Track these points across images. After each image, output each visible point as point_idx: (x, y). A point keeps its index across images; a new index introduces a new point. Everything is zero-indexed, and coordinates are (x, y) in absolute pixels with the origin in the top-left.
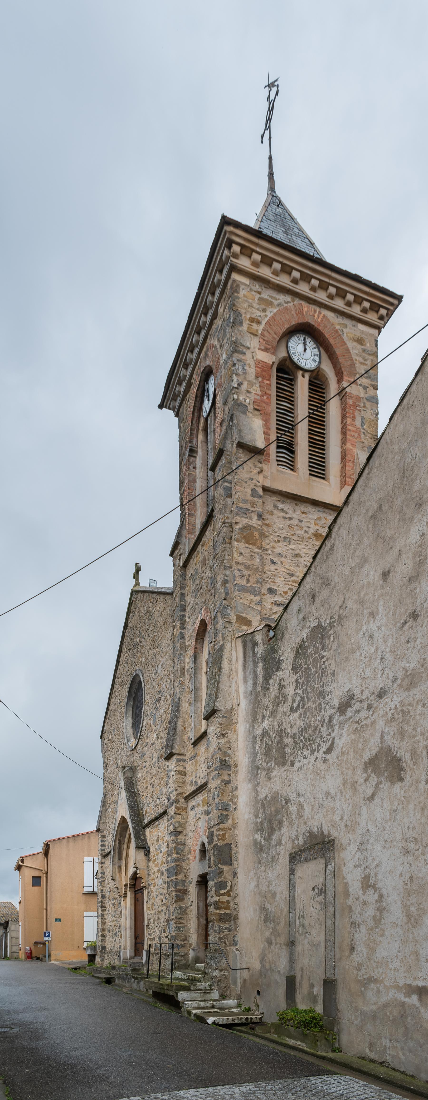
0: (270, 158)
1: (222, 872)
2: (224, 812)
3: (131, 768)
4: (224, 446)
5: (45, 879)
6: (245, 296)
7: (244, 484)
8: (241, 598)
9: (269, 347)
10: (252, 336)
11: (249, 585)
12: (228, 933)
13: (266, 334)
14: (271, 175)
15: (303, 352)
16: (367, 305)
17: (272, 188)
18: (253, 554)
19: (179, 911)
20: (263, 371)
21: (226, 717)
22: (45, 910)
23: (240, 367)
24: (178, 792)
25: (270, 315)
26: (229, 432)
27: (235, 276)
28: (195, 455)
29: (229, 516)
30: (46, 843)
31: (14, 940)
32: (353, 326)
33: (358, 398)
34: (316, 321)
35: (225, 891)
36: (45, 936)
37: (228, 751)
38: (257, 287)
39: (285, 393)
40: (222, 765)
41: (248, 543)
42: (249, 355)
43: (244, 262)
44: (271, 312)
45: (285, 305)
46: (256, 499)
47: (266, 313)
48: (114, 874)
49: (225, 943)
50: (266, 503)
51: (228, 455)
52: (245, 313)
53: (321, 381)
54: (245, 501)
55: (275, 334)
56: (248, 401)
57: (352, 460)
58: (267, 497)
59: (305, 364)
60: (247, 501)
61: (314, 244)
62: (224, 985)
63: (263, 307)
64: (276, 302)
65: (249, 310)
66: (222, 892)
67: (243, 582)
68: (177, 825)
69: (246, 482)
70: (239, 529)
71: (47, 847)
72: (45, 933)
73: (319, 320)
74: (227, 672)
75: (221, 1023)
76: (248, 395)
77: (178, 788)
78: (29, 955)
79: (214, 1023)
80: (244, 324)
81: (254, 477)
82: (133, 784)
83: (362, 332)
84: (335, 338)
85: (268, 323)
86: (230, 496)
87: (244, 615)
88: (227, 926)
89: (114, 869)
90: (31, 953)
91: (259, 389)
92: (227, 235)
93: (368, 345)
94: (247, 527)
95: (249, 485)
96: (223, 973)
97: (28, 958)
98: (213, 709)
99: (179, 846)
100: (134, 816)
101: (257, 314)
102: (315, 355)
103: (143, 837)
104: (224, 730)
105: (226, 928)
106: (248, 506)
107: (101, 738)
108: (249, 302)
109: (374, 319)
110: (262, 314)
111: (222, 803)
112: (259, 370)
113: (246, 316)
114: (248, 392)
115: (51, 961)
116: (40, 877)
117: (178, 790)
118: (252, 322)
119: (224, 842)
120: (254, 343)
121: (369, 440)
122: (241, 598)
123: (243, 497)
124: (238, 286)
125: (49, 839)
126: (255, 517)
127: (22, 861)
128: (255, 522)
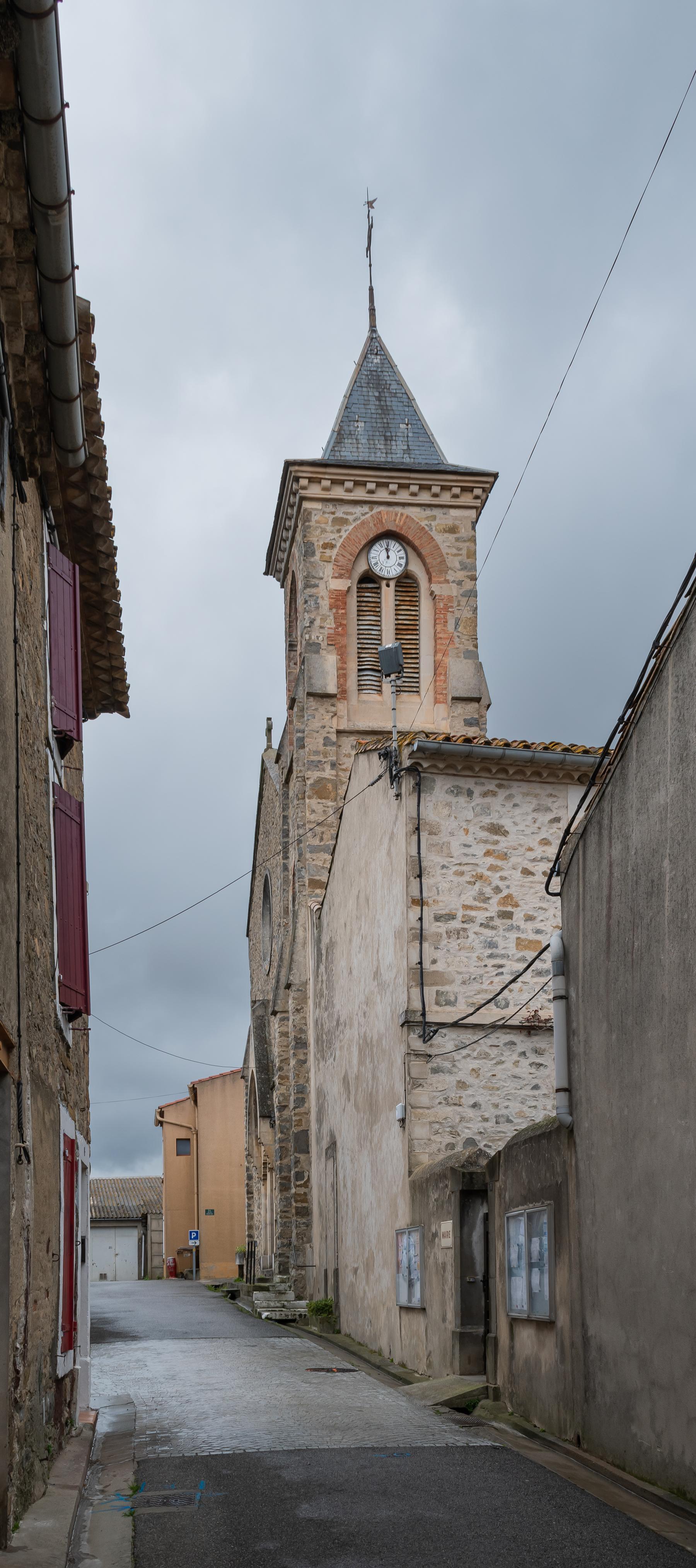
0: (371, 290)
1: (299, 1161)
2: (300, 1096)
3: (263, 1003)
4: (296, 695)
5: (195, 1142)
6: (317, 522)
7: (315, 735)
8: (313, 860)
9: (343, 572)
10: (325, 563)
11: (322, 843)
12: (305, 1228)
13: (340, 558)
14: (372, 310)
15: (386, 560)
16: (457, 491)
17: (373, 328)
18: (326, 809)
19: (285, 1203)
20: (337, 600)
21: (302, 991)
22: (196, 1195)
23: (313, 603)
24: (281, 1058)
25: (344, 535)
26: (301, 677)
27: (306, 505)
28: (295, 649)
29: (302, 768)
30: (191, 1086)
31: (155, 1247)
32: (444, 514)
33: (450, 598)
34: (397, 526)
35: (302, 1182)
36: (191, 1239)
37: (304, 1027)
38: (330, 508)
39: (369, 605)
40: (297, 1043)
41: (321, 798)
42: (322, 585)
43: (315, 491)
44: (346, 531)
45: (363, 518)
46: (329, 748)
47: (341, 534)
48: (250, 1148)
49: (302, 1239)
50: (343, 746)
51: (300, 702)
52: (318, 540)
53: (413, 580)
54: (317, 753)
55: (351, 555)
56: (321, 638)
57: (443, 672)
58: (345, 738)
59: (388, 572)
60: (319, 752)
61: (414, 399)
62: (301, 1285)
63: (338, 527)
64: (351, 518)
65: (323, 536)
66: (298, 1183)
67: (316, 842)
68: (281, 1099)
69: (318, 732)
70: (311, 785)
71: (194, 1090)
72: (191, 1232)
73: (402, 523)
74: (301, 941)
75: (274, 1318)
76: (322, 631)
77: (282, 1053)
78: (172, 1270)
79: (267, 1318)
80: (317, 553)
81: (326, 724)
82: (265, 1026)
83: (456, 518)
84: (421, 537)
85: (343, 546)
86: (303, 747)
87: (317, 878)
88: (304, 1220)
89: (250, 1141)
90: (175, 1267)
91: (333, 621)
92: (293, 474)
93: (463, 530)
94: (320, 780)
95: (321, 734)
96: (299, 1272)
97: (172, 1276)
98: (287, 984)
99: (283, 1124)
100: (262, 1072)
101: (330, 537)
102: (400, 558)
103: (269, 1103)
104: (299, 1005)
105: (304, 1223)
106: (321, 758)
107: (248, 936)
108: (321, 528)
109: (470, 501)
110: (336, 536)
111: (297, 1086)
112: (333, 601)
113: (318, 543)
114: (321, 627)
115: (200, 1279)
116: (189, 1140)
117: (282, 1056)
118: (325, 548)
119: (301, 1128)
120: (328, 570)
121: (466, 642)
122: (313, 860)
123: (315, 749)
124: (310, 514)
125: (196, 1079)
126: (328, 767)
127: (162, 1114)
128: (328, 773)
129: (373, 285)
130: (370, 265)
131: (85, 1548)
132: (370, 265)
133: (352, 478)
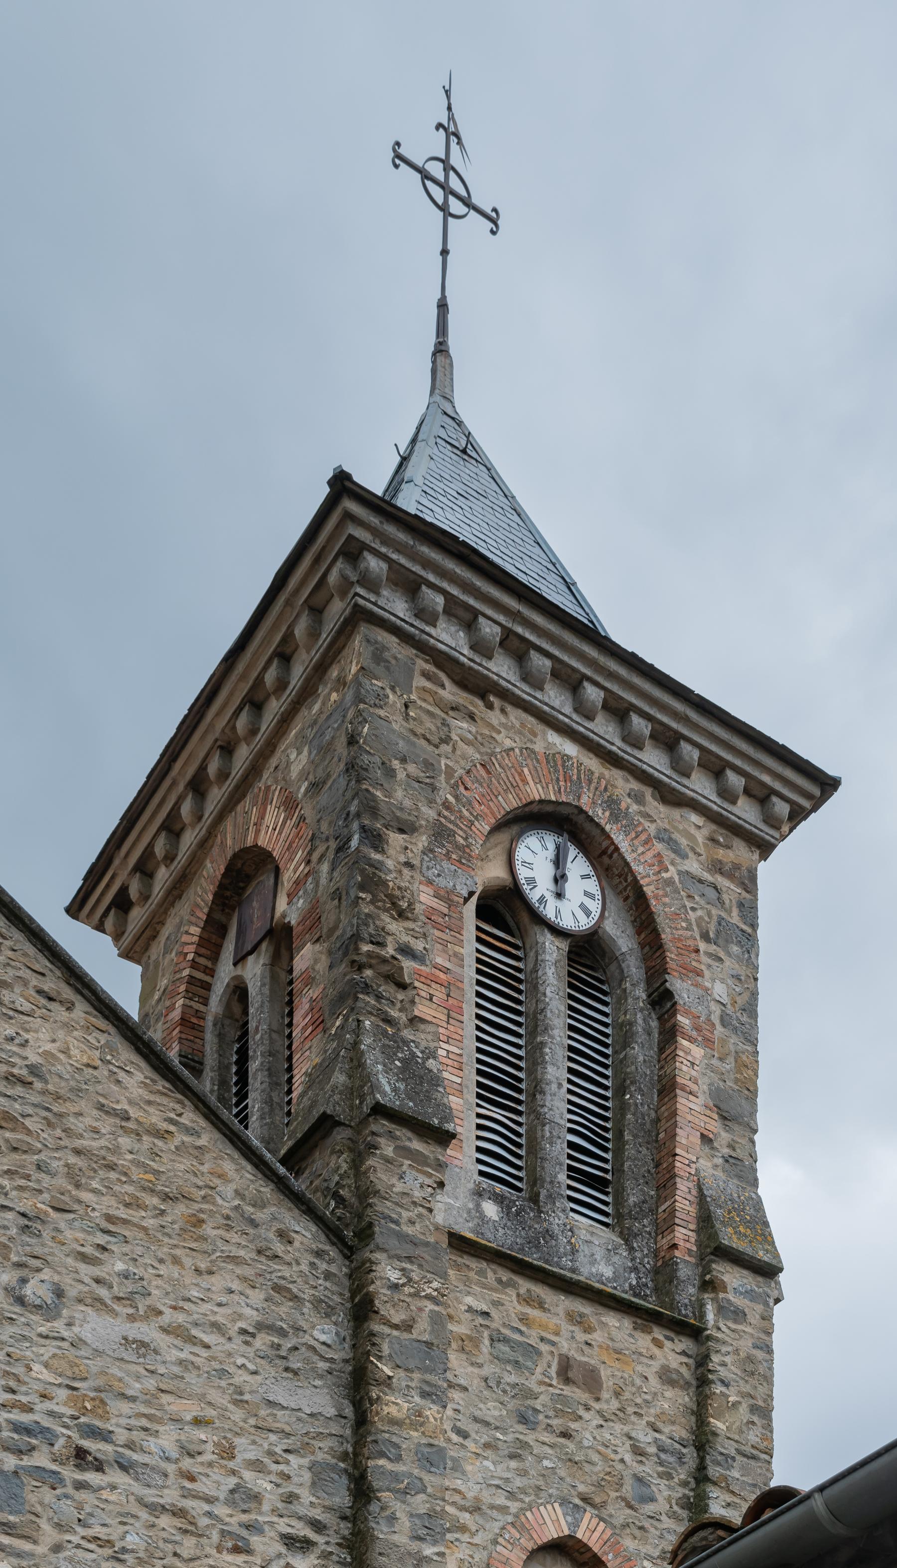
0: (443, 306)
130: (445, 252)
132: (445, 252)
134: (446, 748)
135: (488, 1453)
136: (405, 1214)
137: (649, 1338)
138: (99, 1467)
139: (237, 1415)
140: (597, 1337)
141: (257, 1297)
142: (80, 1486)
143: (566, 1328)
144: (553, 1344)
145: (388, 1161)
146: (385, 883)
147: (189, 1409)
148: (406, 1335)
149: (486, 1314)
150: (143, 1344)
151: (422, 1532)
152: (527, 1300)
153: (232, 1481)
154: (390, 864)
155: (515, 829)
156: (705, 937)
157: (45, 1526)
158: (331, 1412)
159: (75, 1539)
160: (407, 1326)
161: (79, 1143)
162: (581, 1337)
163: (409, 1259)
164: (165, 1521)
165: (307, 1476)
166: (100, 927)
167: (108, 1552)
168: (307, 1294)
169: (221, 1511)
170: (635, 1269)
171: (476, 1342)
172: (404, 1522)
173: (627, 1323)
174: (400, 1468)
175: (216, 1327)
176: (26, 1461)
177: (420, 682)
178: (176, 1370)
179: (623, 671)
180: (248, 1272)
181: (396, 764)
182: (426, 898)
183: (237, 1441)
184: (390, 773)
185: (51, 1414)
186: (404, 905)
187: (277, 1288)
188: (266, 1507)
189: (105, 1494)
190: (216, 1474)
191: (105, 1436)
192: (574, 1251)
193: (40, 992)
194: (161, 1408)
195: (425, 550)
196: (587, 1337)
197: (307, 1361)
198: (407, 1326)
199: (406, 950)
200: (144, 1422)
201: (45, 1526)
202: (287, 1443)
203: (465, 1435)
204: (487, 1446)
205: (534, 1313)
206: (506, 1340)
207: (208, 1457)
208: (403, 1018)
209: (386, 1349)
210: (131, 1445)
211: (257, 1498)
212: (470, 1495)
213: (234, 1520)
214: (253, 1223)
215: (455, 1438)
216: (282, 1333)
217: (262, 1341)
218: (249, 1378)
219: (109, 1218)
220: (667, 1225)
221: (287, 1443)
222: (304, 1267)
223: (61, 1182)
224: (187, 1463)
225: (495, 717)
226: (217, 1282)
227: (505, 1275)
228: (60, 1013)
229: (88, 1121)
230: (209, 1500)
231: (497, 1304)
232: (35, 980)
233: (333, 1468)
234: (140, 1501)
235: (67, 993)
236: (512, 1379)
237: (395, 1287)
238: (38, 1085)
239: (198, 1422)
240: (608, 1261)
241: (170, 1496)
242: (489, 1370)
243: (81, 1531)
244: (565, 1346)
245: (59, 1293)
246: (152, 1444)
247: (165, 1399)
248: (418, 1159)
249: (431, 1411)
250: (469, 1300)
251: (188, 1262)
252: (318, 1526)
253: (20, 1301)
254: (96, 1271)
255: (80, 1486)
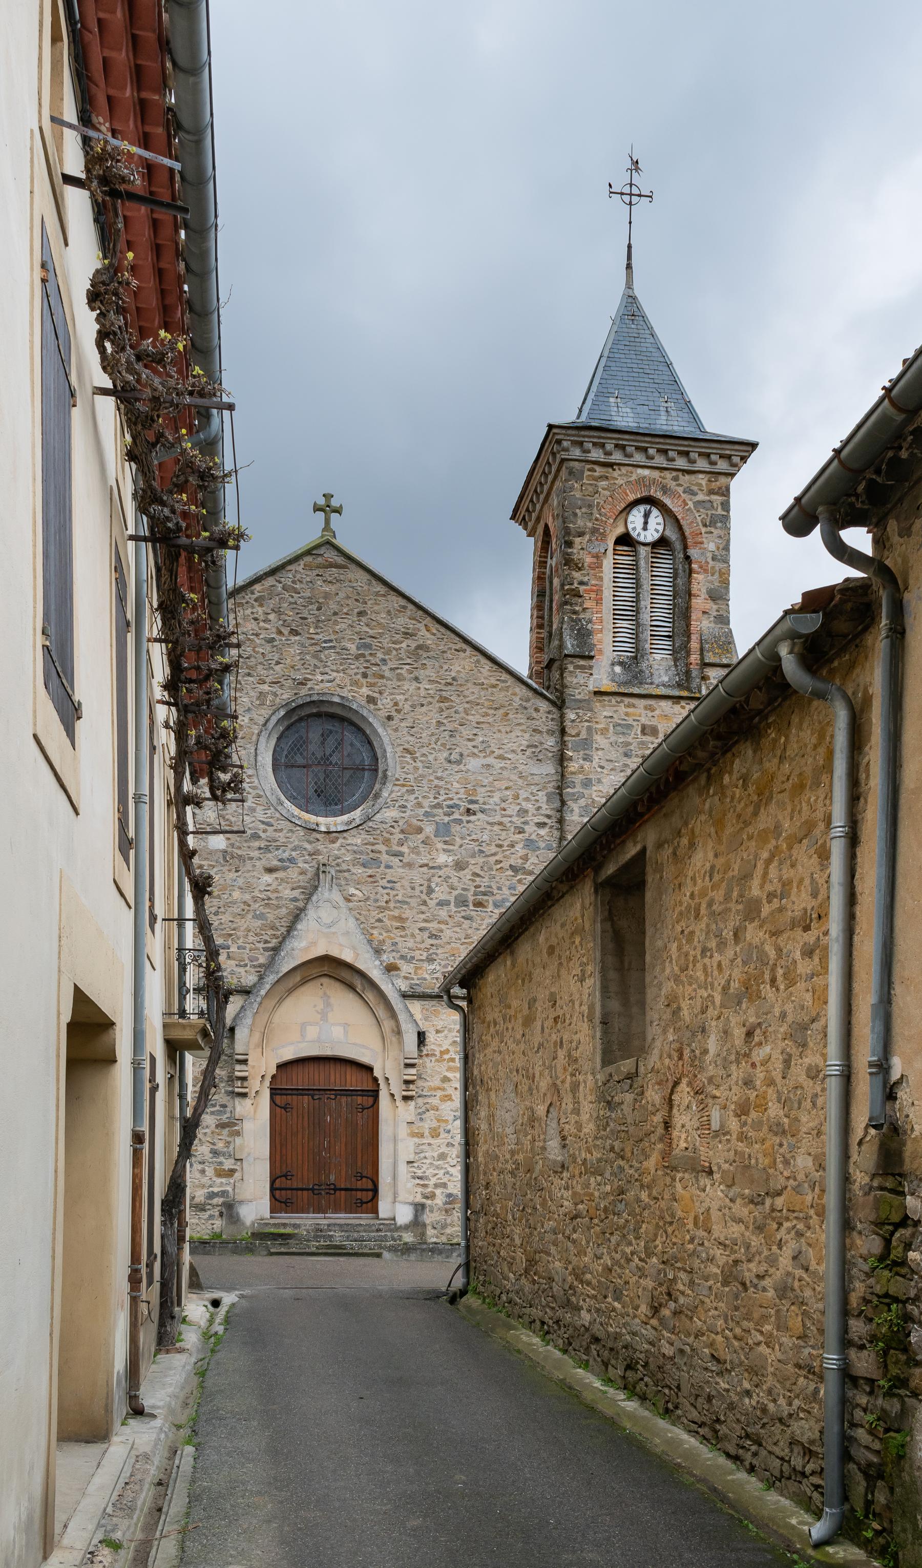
0: (629, 247)
17: (629, 285)
129: (638, 291)
130: (630, 223)
131: (219, 941)
132: (630, 223)
133: (636, 444)
134: (597, 495)
135: (613, 772)
136: (577, 691)
137: (679, 706)
138: (474, 814)
139: (520, 782)
140: (657, 712)
141: (527, 736)
142: (468, 822)
143: (643, 712)
144: (638, 721)
145: (571, 672)
146: (573, 560)
147: (504, 784)
148: (577, 738)
149: (612, 717)
150: (489, 765)
151: (583, 813)
152: (628, 706)
153: (519, 807)
154: (575, 551)
155: (624, 514)
156: (705, 525)
157: (458, 839)
158: (554, 771)
159: (466, 841)
160: (578, 735)
161: (467, 699)
162: (650, 714)
163: (579, 708)
164: (496, 828)
165: (545, 798)
166: (520, 524)
167: (477, 843)
168: (545, 729)
169: (515, 819)
170: (678, 674)
171: (607, 729)
172: (576, 810)
173: (670, 703)
174: (575, 790)
175: (513, 751)
176: (452, 818)
177: (587, 473)
178: (500, 771)
179: (662, 440)
180: (524, 727)
181: (578, 511)
182: (588, 560)
183: (520, 792)
184: (575, 515)
185: (460, 799)
186: (580, 565)
187: (534, 730)
188: (530, 814)
189: (476, 823)
190: (513, 806)
191: (476, 802)
192: (652, 675)
193: (456, 650)
194: (494, 787)
195: (583, 433)
196: (653, 714)
197: (545, 755)
198: (578, 735)
199: (581, 583)
200: (489, 794)
201: (458, 839)
202: (538, 788)
203: (602, 768)
204: (612, 770)
205: (630, 710)
206: (620, 725)
207: (511, 800)
208: (581, 609)
209: (570, 746)
210: (484, 803)
211: (526, 811)
212: (605, 791)
213: (518, 821)
214: (526, 708)
215: (599, 770)
216: (536, 746)
217: (530, 750)
218: (524, 767)
219: (478, 723)
220: (688, 654)
221: (538, 788)
222: (544, 719)
223: (463, 715)
224: (503, 805)
225: (616, 474)
226: (513, 734)
227: (619, 699)
228: (462, 654)
229: (471, 690)
230: (510, 816)
231: (616, 711)
232: (454, 647)
233: (554, 793)
234: (488, 823)
235: (464, 646)
236: (621, 740)
237: (573, 721)
238: (455, 683)
239: (506, 788)
240: (666, 674)
241: (498, 818)
242: (613, 739)
243: (469, 838)
244: (644, 720)
245: (461, 755)
246: (491, 801)
247: (496, 783)
248: (582, 667)
249: (587, 765)
250: (605, 713)
251: (503, 730)
252: (549, 817)
253: (450, 762)
254: (473, 743)
255: (468, 822)
